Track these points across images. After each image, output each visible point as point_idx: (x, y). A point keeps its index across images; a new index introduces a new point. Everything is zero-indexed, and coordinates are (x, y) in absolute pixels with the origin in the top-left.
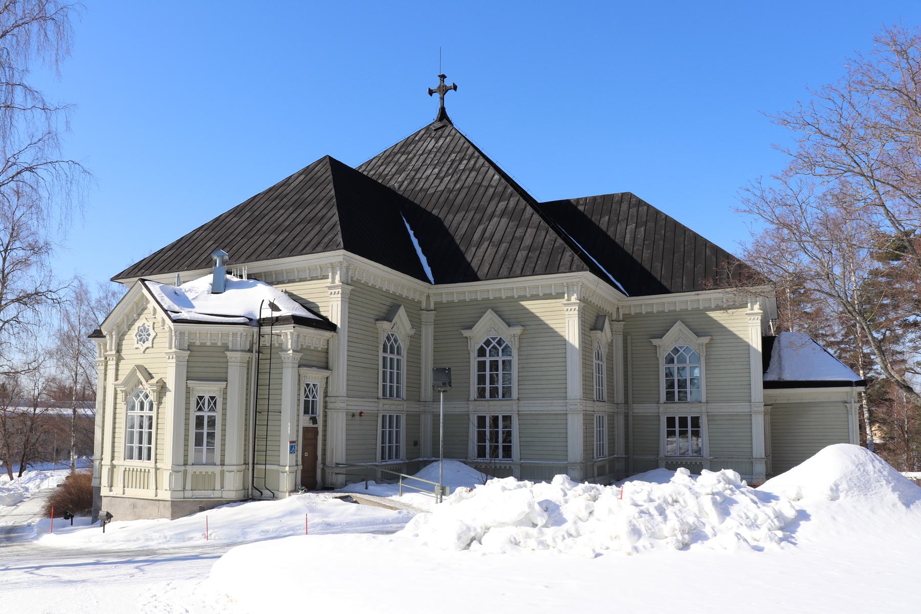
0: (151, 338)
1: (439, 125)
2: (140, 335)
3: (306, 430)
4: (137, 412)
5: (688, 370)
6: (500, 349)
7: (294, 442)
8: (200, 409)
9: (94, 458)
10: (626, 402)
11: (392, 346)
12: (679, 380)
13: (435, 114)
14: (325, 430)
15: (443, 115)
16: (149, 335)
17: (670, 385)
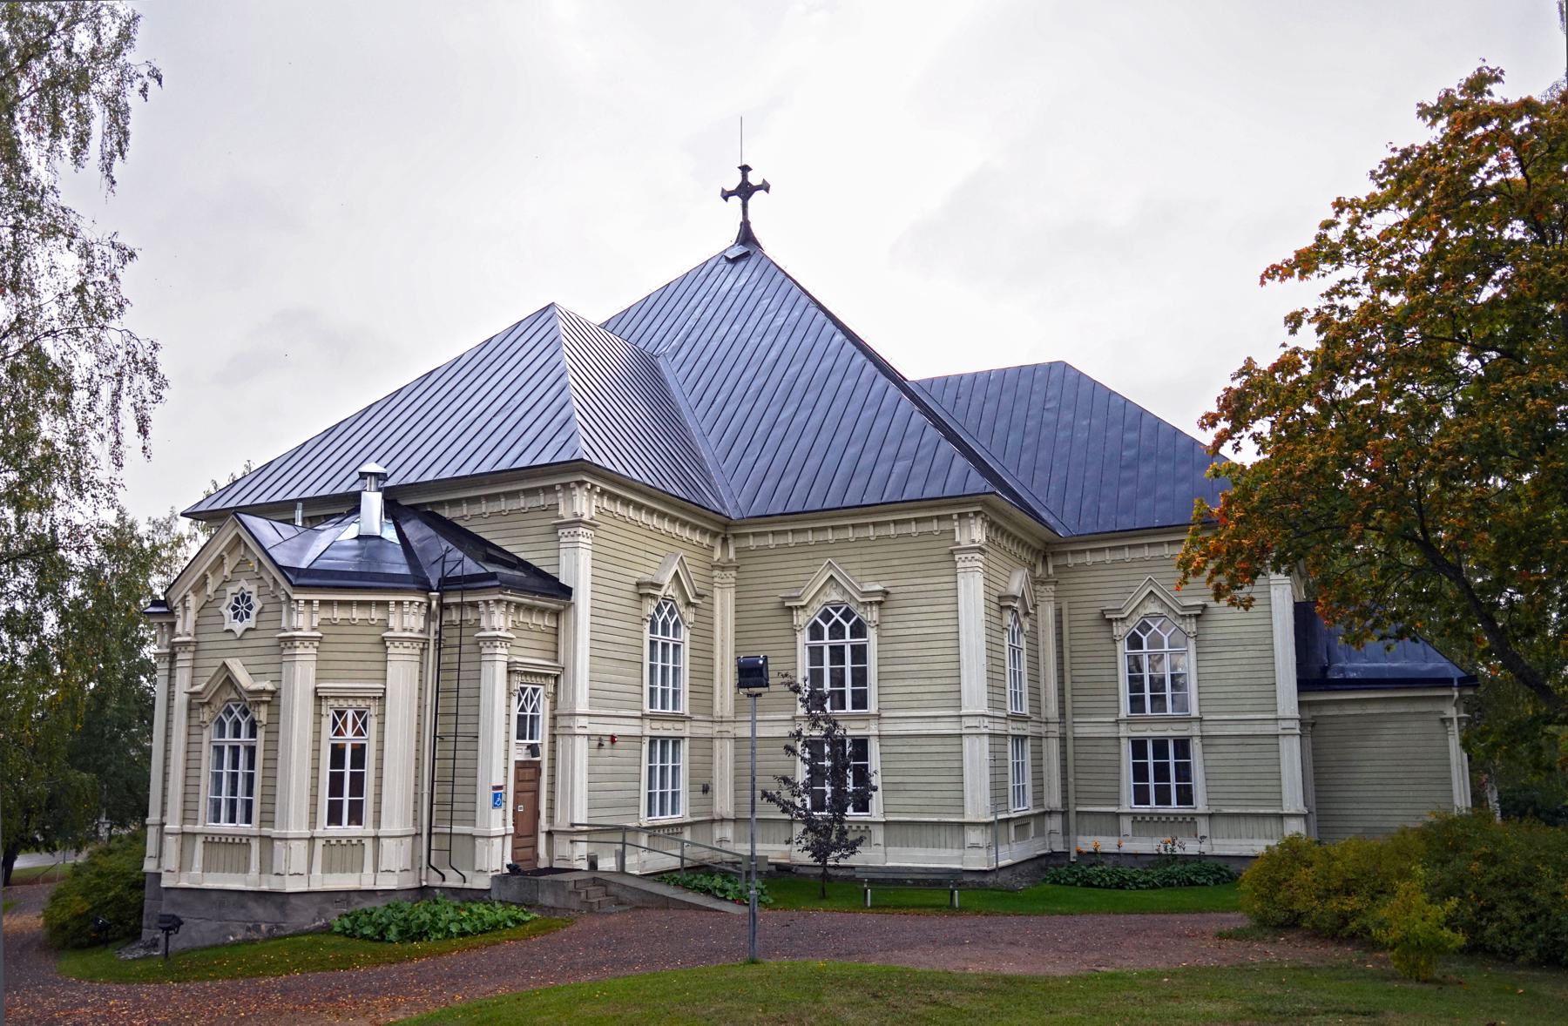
0: (253, 613)
1: (738, 251)
2: (237, 601)
3: (520, 765)
4: (228, 738)
5: (1167, 658)
6: (847, 627)
7: (500, 788)
8: (339, 733)
9: (148, 821)
10: (1062, 715)
11: (665, 623)
12: (1151, 677)
13: (734, 232)
14: (553, 767)
15: (746, 236)
16: (250, 607)
17: (1136, 684)
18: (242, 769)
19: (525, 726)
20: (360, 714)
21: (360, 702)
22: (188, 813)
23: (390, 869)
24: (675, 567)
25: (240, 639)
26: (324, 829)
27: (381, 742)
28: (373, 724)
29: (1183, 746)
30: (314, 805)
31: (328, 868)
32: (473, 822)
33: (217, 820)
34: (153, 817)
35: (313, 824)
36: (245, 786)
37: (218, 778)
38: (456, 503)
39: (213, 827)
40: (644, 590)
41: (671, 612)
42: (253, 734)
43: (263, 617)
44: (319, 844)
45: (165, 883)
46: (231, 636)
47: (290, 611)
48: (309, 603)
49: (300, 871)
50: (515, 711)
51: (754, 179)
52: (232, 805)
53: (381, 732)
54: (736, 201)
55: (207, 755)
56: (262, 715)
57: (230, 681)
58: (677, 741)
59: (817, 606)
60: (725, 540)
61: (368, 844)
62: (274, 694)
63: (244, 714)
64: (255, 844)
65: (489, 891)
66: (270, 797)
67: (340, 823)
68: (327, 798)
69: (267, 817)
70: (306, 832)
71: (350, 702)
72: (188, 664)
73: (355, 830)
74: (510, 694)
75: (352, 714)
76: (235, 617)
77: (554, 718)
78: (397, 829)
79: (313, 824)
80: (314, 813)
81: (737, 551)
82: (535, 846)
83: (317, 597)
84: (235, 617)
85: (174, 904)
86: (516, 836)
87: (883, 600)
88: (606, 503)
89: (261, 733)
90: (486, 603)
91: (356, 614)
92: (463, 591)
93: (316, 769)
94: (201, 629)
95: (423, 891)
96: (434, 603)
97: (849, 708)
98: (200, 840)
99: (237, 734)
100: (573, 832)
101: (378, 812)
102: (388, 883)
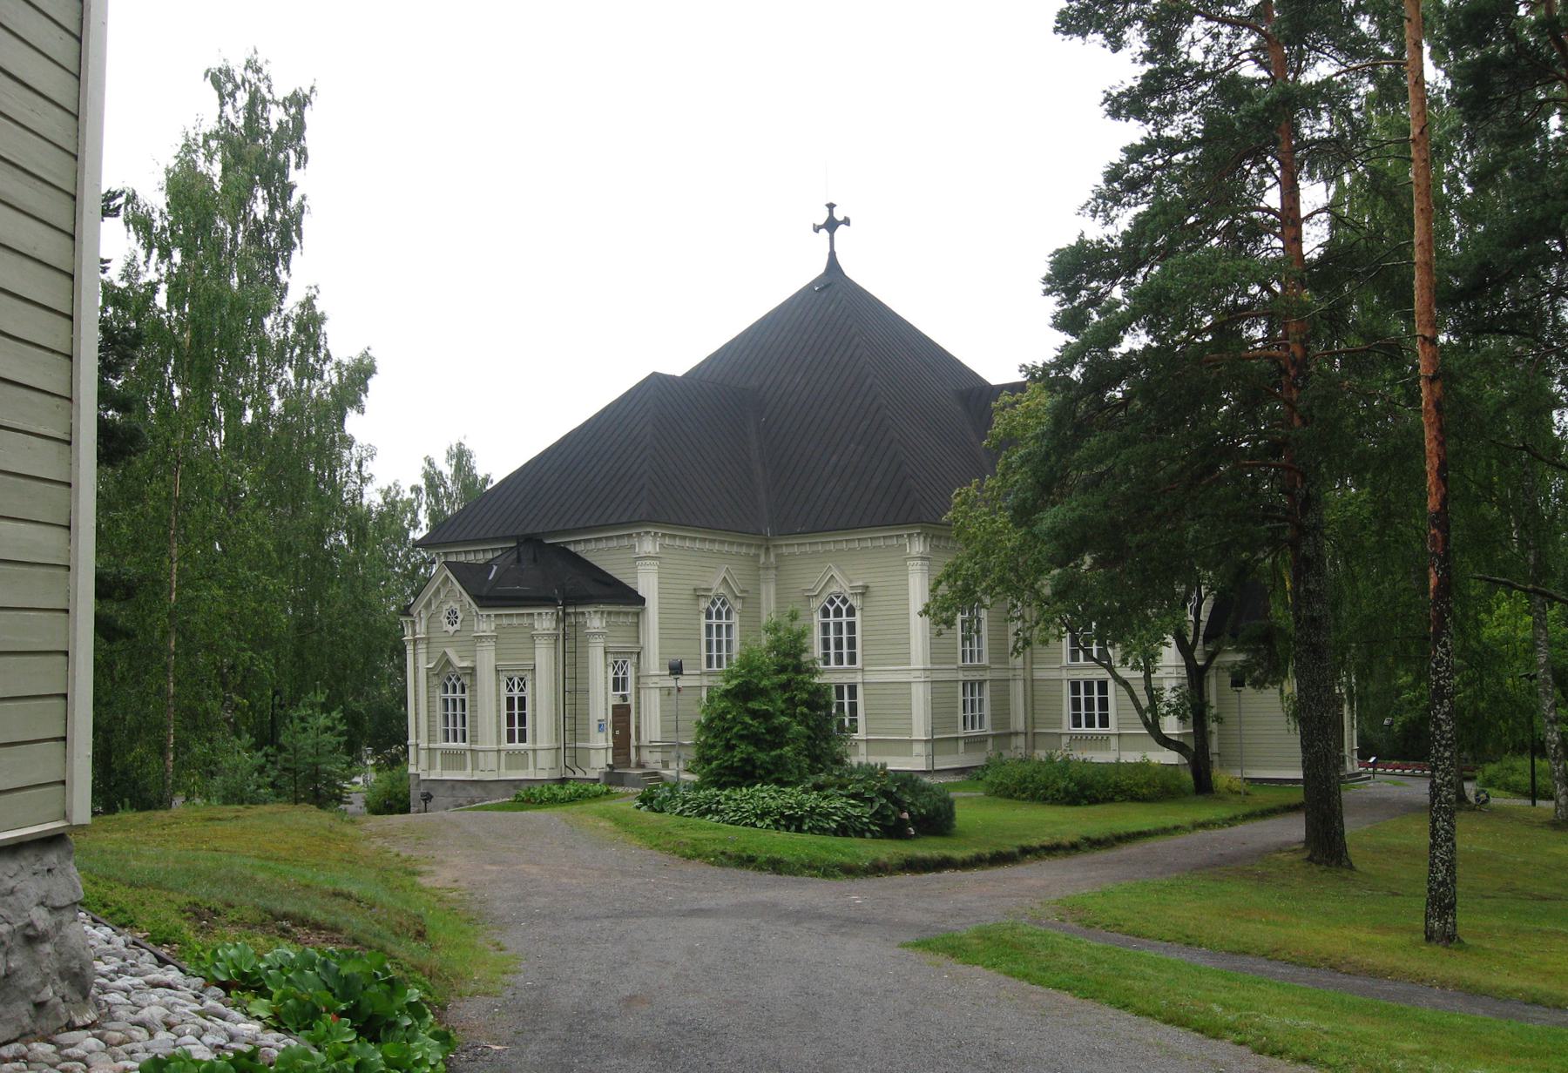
15: (833, 264)
18: (459, 712)
19: (618, 684)
24: (723, 575)
26: (505, 745)
27: (534, 695)
28: (529, 685)
29: (853, 689)
30: (499, 732)
31: (509, 767)
32: (587, 740)
34: (411, 741)
35: (499, 742)
36: (458, 720)
37: (446, 717)
38: (576, 542)
39: (445, 745)
40: (698, 594)
41: (723, 604)
44: (503, 754)
50: (611, 675)
51: (839, 216)
54: (824, 233)
55: (439, 705)
56: (466, 680)
57: (448, 662)
58: (981, 683)
59: (825, 595)
60: (767, 549)
62: (473, 669)
63: (455, 683)
66: (474, 727)
70: (495, 747)
73: (522, 745)
74: (607, 666)
77: (638, 678)
78: (546, 745)
79: (499, 742)
81: (777, 556)
82: (629, 754)
86: (615, 749)
87: (865, 592)
88: (667, 541)
91: (515, 621)
92: (576, 605)
93: (499, 711)
97: (845, 665)
100: (652, 747)
101: (535, 736)
102: (544, 775)
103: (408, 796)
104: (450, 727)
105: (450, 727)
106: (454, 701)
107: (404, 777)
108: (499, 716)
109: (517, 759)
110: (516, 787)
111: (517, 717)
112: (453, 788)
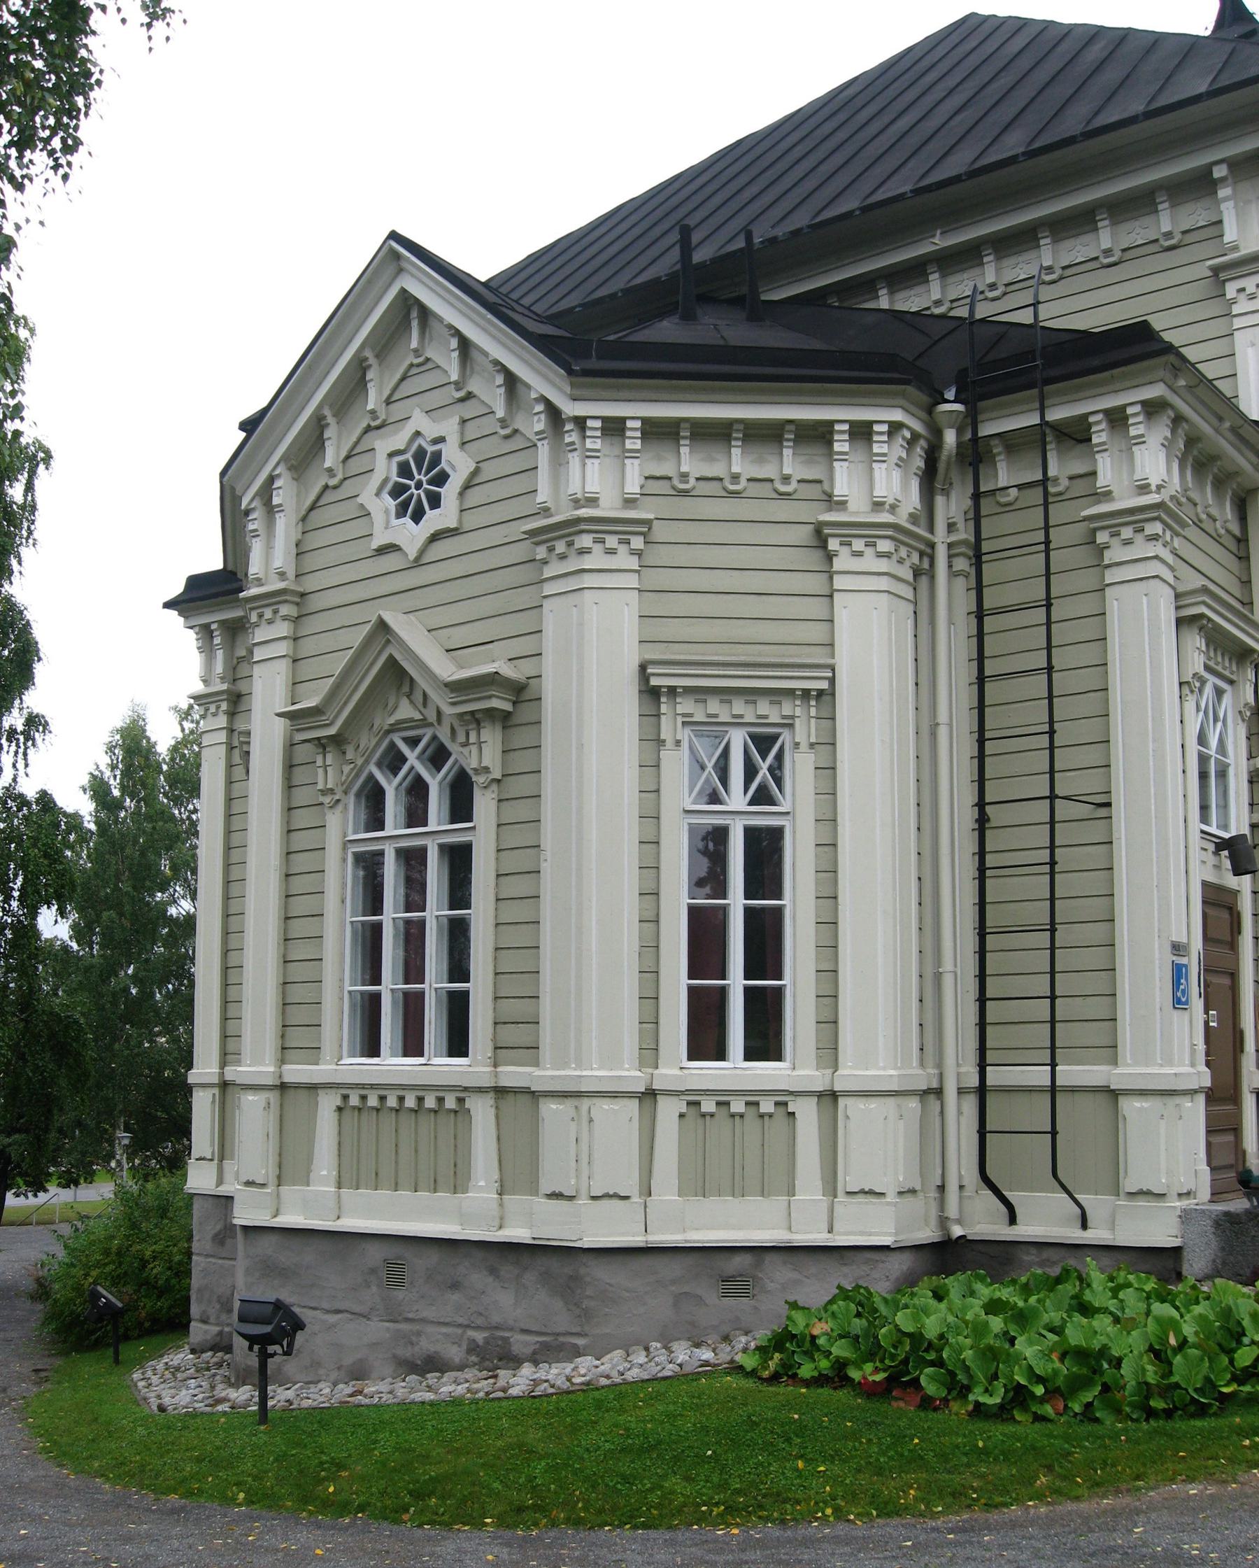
0: (449, 492)
2: (404, 470)
16: (441, 479)
20: (763, 742)
21: (764, 707)
22: (295, 1034)
23: (860, 1178)
25: (418, 563)
26: (679, 1069)
27: (829, 820)
31: (697, 1183)
32: (1111, 1051)
33: (372, 1048)
35: (650, 1052)
37: (371, 939)
39: (357, 1067)
42: (461, 808)
43: (475, 497)
44: (669, 1110)
45: (244, 1215)
46: (390, 562)
47: (558, 463)
48: (614, 428)
49: (614, 1183)
52: (412, 1007)
53: (829, 792)
56: (484, 753)
57: (396, 676)
61: (806, 1112)
62: (521, 692)
64: (482, 1111)
65: (1177, 1251)
66: (520, 983)
67: (721, 1055)
68: (684, 981)
69: (510, 1035)
70: (632, 1076)
71: (739, 707)
72: (282, 648)
75: (752, 717)
76: (402, 511)
79: (650, 1052)
80: (651, 1022)
83: (635, 411)
84: (402, 511)
85: (269, 1269)
89: (484, 804)
90: (1117, 419)
93: (652, 894)
94: (311, 562)
95: (947, 1255)
96: (950, 437)
98: (328, 1103)
99: (416, 816)
101: (830, 1023)
103: (182, 1271)
104: (390, 984)
105: (390, 984)
106: (413, 860)
107: (172, 1210)
108: (651, 999)
109: (734, 1141)
110: (734, 1285)
111: (737, 972)
112: (394, 1274)
